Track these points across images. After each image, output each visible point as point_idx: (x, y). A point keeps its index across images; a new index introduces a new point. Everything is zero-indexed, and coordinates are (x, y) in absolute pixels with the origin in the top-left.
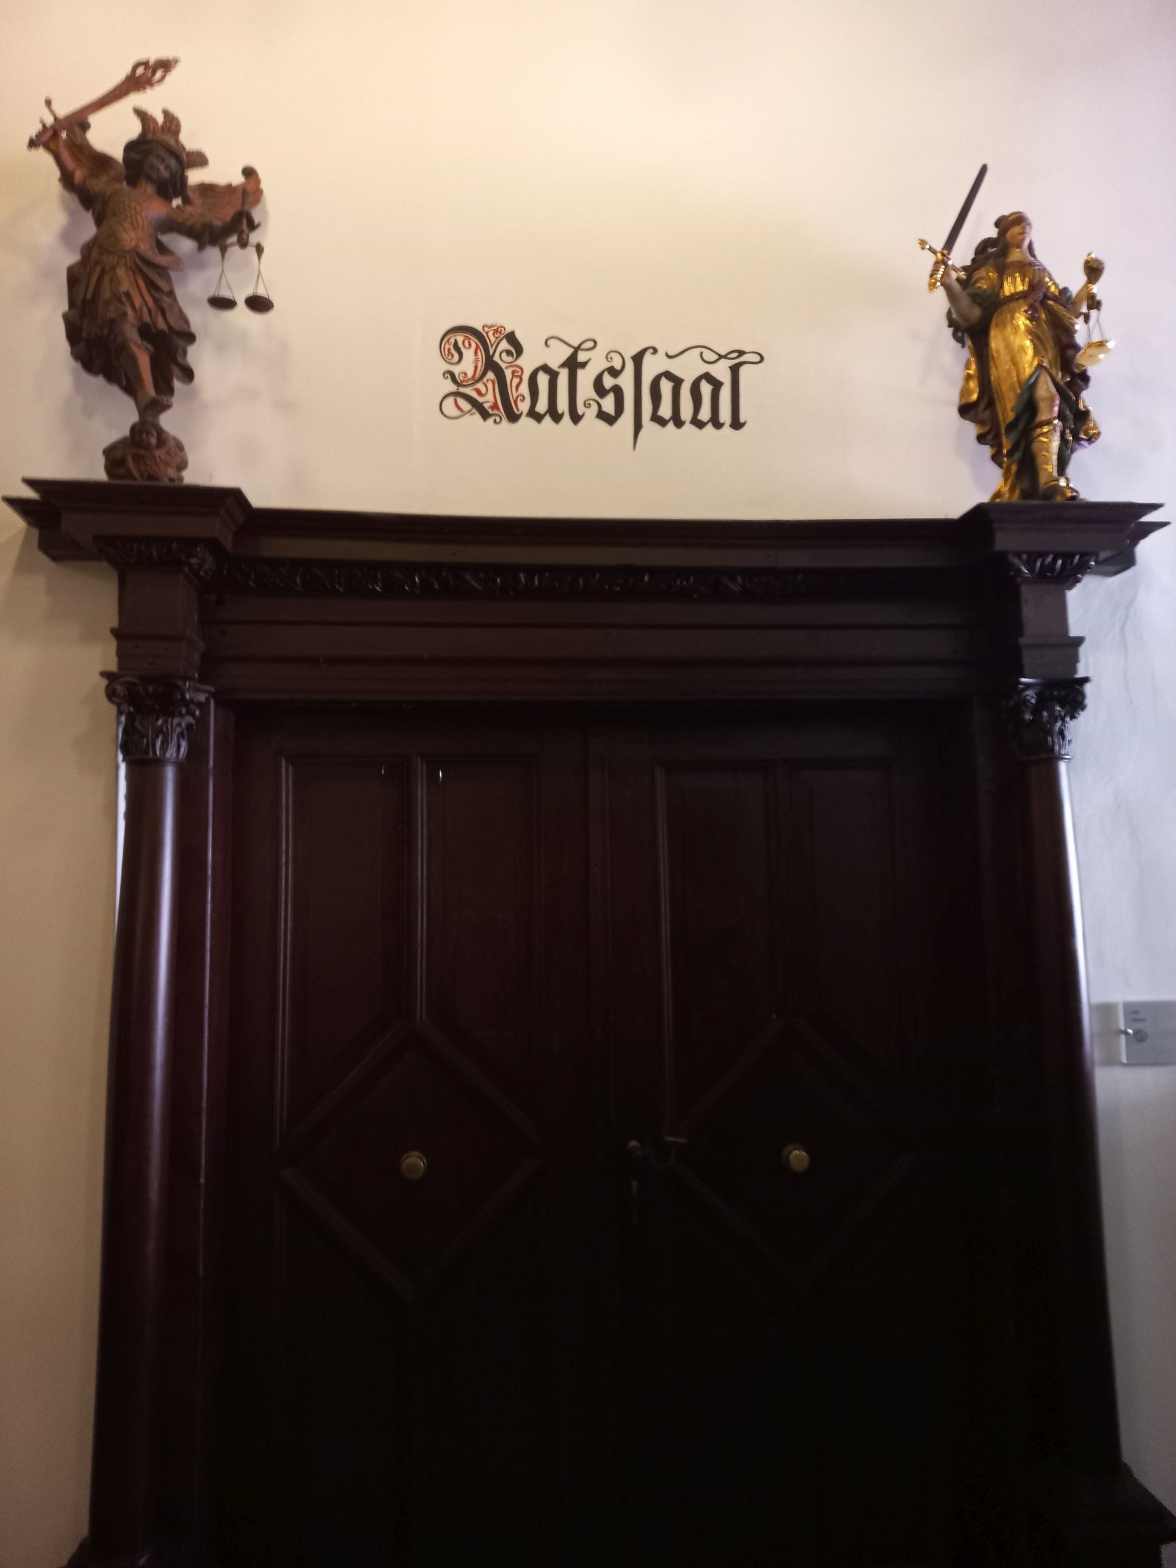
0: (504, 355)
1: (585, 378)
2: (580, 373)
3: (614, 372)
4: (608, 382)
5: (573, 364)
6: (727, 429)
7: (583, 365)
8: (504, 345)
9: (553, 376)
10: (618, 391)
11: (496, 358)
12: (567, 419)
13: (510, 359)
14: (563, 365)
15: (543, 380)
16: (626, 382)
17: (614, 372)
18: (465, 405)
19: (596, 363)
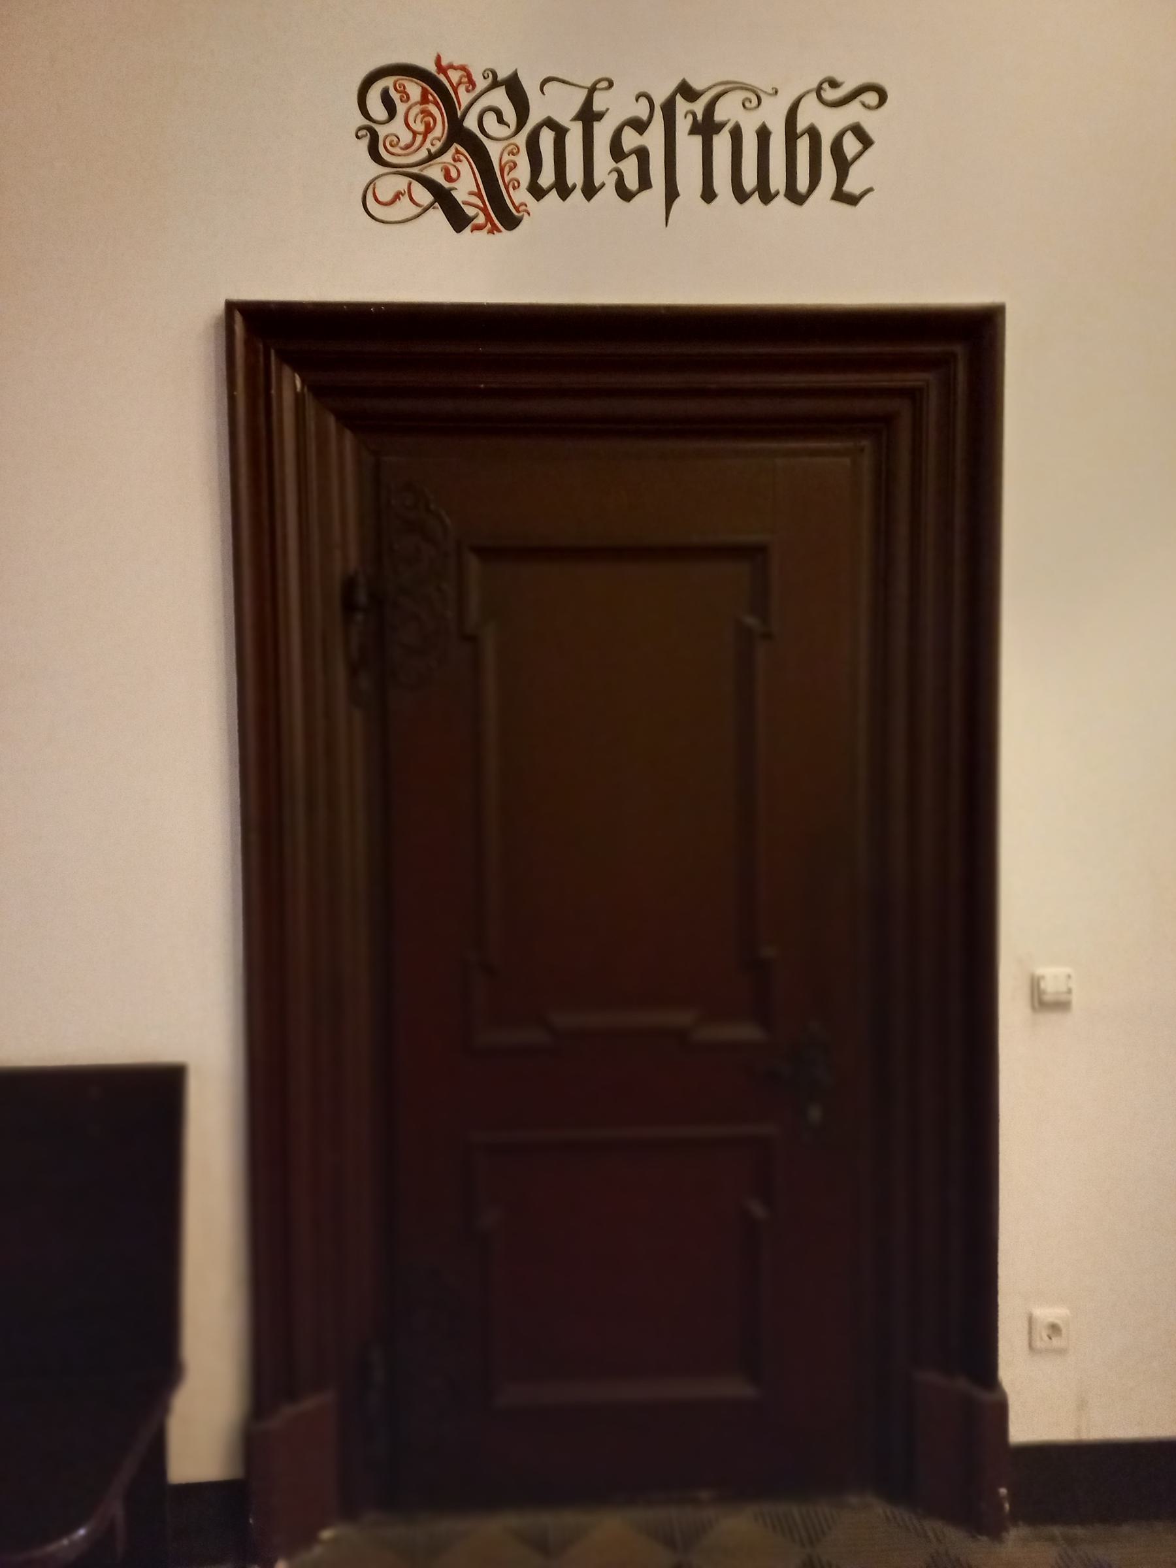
0: (490, 120)
1: (602, 133)
2: (598, 127)
3: (640, 126)
4: (630, 140)
5: (588, 116)
6: (781, 202)
7: (600, 116)
8: (499, 98)
9: (561, 133)
10: (642, 155)
11: (471, 123)
12: (577, 195)
13: (503, 132)
14: (577, 118)
15: (547, 139)
16: (654, 139)
17: (640, 126)
18: (424, 196)
19: (617, 107)
